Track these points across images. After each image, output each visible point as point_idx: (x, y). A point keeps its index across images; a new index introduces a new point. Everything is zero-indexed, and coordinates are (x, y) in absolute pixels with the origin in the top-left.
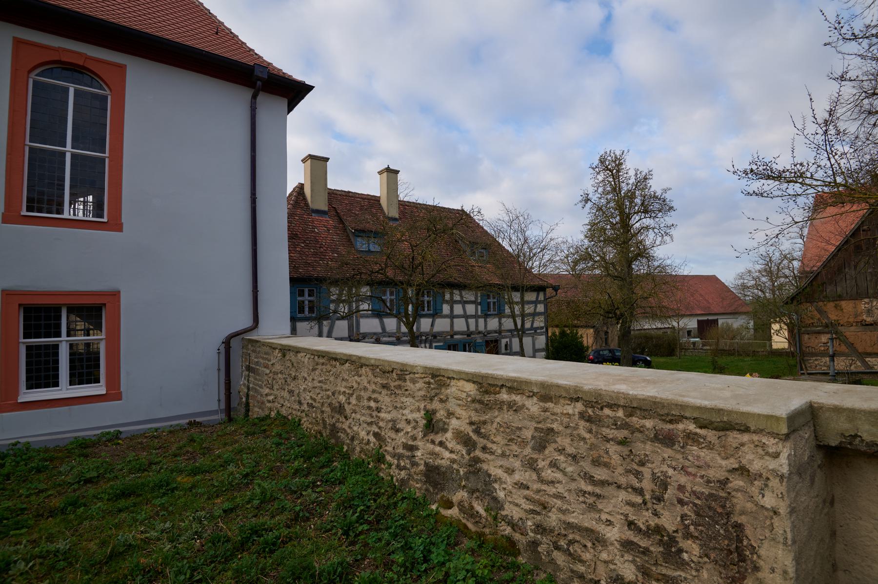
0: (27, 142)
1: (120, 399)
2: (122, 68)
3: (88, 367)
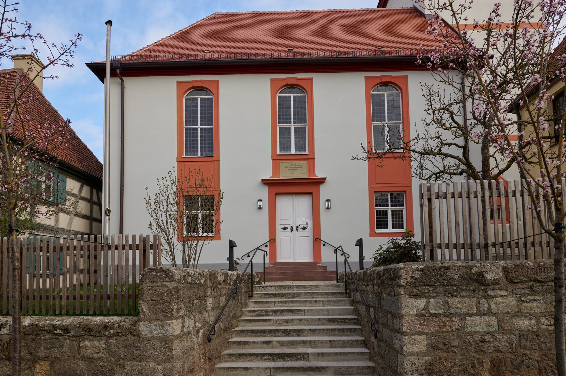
0: (184, 126)
3: (384, 221)
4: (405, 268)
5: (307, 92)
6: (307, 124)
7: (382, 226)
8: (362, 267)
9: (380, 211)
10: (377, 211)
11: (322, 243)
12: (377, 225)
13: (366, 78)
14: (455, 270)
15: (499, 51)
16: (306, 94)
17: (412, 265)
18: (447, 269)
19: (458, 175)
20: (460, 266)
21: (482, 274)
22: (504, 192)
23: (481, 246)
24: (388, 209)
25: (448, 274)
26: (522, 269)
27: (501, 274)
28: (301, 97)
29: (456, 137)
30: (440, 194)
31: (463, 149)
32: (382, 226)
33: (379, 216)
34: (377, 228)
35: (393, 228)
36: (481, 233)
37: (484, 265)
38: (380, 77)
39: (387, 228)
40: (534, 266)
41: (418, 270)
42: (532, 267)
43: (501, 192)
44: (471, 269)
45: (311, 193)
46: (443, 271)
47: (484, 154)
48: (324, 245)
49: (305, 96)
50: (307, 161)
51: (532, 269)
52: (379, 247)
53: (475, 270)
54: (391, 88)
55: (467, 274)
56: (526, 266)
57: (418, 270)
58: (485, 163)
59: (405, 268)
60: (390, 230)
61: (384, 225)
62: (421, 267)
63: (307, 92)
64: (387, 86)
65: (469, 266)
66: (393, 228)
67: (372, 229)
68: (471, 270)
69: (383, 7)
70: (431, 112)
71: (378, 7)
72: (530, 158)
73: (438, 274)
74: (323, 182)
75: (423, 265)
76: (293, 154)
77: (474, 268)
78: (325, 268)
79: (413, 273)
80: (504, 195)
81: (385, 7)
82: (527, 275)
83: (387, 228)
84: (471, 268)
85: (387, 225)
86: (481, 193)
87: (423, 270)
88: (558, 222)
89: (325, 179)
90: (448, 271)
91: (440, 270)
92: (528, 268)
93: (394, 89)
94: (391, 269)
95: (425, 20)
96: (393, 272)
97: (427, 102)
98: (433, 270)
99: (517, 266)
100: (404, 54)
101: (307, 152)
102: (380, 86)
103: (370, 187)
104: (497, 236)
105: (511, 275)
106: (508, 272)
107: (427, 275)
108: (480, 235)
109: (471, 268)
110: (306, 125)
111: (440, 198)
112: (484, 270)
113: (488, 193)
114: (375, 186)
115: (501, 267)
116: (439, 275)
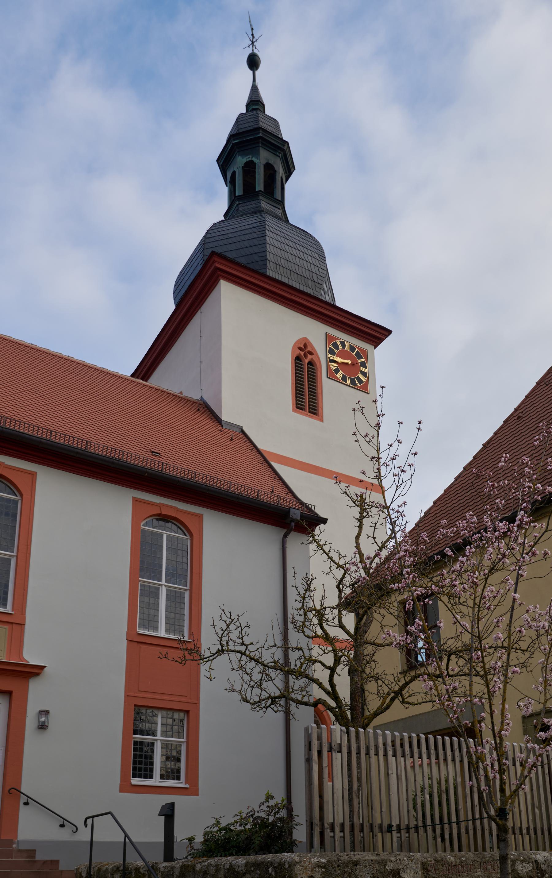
1: (198, 795)
2: (33, 475)
4: (301, 861)
5: (21, 495)
6: (15, 554)
7: (143, 772)
8: (169, 855)
9: (142, 743)
10: (136, 743)
11: (23, 799)
12: (134, 769)
13: (136, 501)
14: (366, 866)
15: (376, 542)
16: (19, 498)
17: (310, 858)
18: (356, 865)
19: (310, 706)
20: (372, 861)
21: (399, 873)
22: (409, 752)
23: (384, 830)
24: (157, 740)
25: (357, 873)
26: (442, 865)
27: (420, 872)
28: (8, 500)
29: (325, 653)
30: (333, 745)
31: (330, 671)
32: (143, 772)
33: (138, 753)
34: (134, 776)
35: (162, 777)
36: (383, 810)
37: (400, 860)
38: (159, 505)
39: (151, 777)
40: (456, 862)
41: (319, 865)
42: (454, 863)
43: (406, 751)
44: (385, 865)
45: (9, 693)
46: (351, 868)
47: (354, 683)
48: (26, 804)
49: (16, 502)
50: (7, 627)
51: (454, 866)
52: (214, 822)
53: (390, 866)
54: (174, 527)
55: (380, 873)
56: (447, 862)
57: (319, 866)
58: (355, 697)
59: (301, 861)
60: (156, 781)
61: (146, 770)
62: (323, 861)
63: (21, 495)
64: (168, 522)
65: (382, 860)
66: (162, 777)
67: (124, 779)
68: (385, 867)
69: (142, 379)
70: (302, 612)
71: (133, 375)
72: (408, 697)
73: (345, 872)
74: (38, 674)
75: (325, 858)
76: (162, 636)
77: (389, 864)
78: (31, 853)
79: (312, 870)
80: (409, 756)
81: (146, 381)
82: (448, 875)
83: (151, 777)
84: (384, 863)
85: (152, 770)
86: (382, 749)
87: (325, 866)
88: (502, 807)
89: (42, 667)
90: (358, 867)
91: (347, 867)
92: (449, 864)
93: (179, 530)
94: (271, 863)
95: (221, 428)
96: (275, 868)
97: (299, 599)
98: (338, 866)
99: (437, 861)
100: (200, 480)
101: (9, 609)
102: (157, 519)
103: (128, 696)
104: (402, 815)
105: (431, 874)
106: (427, 870)
107: (330, 873)
108: (381, 812)
109: (384, 863)
110: (13, 556)
111: (333, 752)
112: (400, 867)
113: (391, 750)
114: (136, 695)
115: (419, 863)
116: (346, 874)
